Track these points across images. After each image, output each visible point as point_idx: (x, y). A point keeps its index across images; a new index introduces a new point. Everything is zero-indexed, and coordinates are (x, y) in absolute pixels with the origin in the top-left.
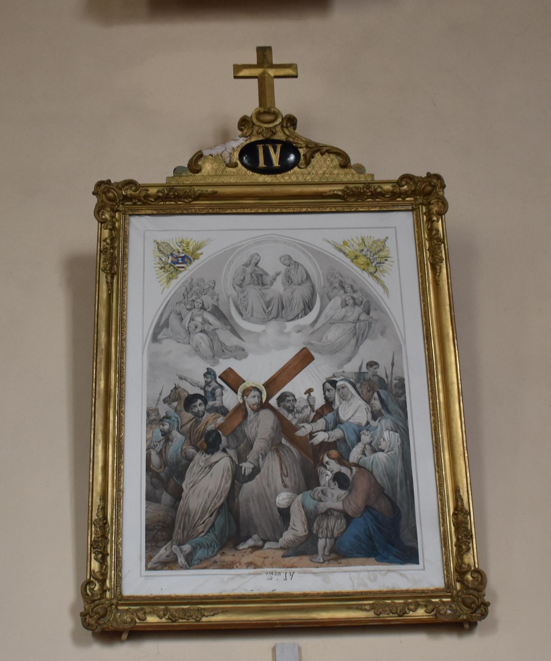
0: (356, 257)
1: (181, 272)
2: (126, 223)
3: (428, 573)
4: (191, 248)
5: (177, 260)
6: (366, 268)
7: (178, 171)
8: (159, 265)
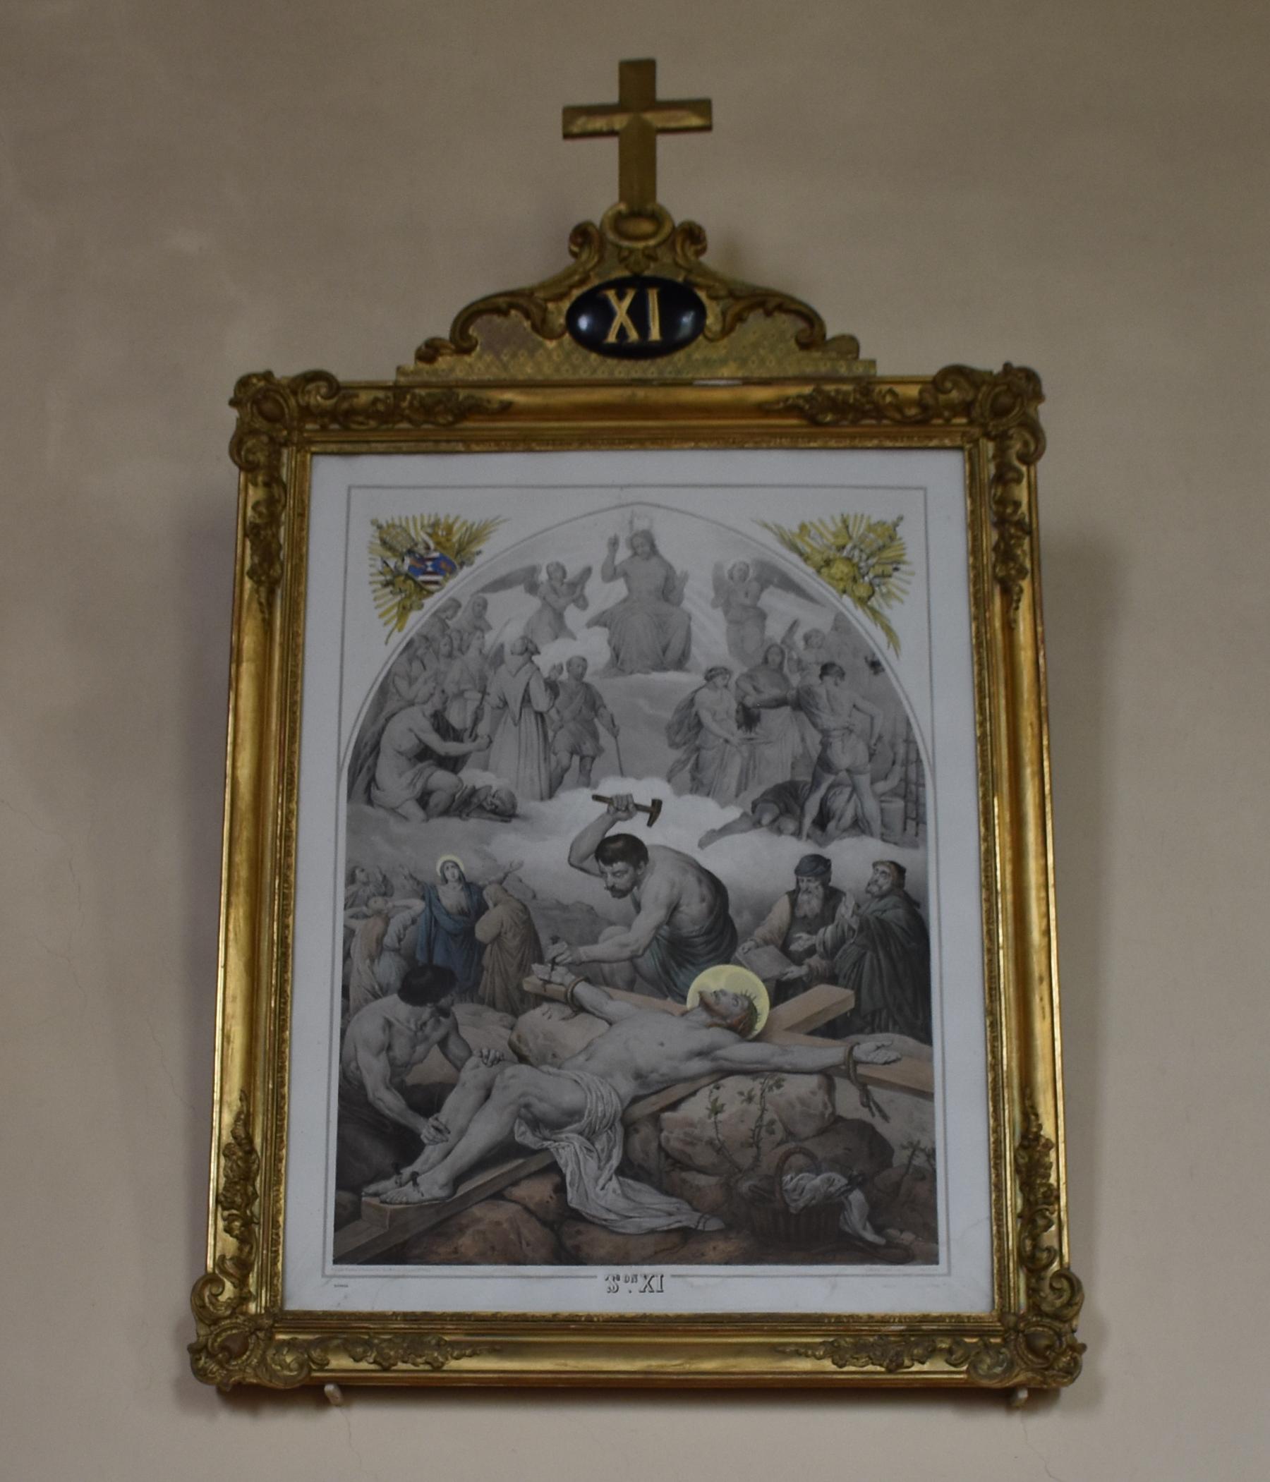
0: (828, 563)
1: (431, 593)
2: (302, 474)
3: (958, 1278)
4: (455, 538)
5: (418, 563)
6: (849, 589)
7: (429, 352)
8: (382, 578)
